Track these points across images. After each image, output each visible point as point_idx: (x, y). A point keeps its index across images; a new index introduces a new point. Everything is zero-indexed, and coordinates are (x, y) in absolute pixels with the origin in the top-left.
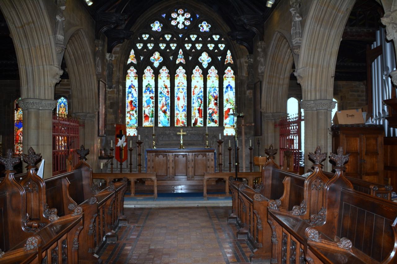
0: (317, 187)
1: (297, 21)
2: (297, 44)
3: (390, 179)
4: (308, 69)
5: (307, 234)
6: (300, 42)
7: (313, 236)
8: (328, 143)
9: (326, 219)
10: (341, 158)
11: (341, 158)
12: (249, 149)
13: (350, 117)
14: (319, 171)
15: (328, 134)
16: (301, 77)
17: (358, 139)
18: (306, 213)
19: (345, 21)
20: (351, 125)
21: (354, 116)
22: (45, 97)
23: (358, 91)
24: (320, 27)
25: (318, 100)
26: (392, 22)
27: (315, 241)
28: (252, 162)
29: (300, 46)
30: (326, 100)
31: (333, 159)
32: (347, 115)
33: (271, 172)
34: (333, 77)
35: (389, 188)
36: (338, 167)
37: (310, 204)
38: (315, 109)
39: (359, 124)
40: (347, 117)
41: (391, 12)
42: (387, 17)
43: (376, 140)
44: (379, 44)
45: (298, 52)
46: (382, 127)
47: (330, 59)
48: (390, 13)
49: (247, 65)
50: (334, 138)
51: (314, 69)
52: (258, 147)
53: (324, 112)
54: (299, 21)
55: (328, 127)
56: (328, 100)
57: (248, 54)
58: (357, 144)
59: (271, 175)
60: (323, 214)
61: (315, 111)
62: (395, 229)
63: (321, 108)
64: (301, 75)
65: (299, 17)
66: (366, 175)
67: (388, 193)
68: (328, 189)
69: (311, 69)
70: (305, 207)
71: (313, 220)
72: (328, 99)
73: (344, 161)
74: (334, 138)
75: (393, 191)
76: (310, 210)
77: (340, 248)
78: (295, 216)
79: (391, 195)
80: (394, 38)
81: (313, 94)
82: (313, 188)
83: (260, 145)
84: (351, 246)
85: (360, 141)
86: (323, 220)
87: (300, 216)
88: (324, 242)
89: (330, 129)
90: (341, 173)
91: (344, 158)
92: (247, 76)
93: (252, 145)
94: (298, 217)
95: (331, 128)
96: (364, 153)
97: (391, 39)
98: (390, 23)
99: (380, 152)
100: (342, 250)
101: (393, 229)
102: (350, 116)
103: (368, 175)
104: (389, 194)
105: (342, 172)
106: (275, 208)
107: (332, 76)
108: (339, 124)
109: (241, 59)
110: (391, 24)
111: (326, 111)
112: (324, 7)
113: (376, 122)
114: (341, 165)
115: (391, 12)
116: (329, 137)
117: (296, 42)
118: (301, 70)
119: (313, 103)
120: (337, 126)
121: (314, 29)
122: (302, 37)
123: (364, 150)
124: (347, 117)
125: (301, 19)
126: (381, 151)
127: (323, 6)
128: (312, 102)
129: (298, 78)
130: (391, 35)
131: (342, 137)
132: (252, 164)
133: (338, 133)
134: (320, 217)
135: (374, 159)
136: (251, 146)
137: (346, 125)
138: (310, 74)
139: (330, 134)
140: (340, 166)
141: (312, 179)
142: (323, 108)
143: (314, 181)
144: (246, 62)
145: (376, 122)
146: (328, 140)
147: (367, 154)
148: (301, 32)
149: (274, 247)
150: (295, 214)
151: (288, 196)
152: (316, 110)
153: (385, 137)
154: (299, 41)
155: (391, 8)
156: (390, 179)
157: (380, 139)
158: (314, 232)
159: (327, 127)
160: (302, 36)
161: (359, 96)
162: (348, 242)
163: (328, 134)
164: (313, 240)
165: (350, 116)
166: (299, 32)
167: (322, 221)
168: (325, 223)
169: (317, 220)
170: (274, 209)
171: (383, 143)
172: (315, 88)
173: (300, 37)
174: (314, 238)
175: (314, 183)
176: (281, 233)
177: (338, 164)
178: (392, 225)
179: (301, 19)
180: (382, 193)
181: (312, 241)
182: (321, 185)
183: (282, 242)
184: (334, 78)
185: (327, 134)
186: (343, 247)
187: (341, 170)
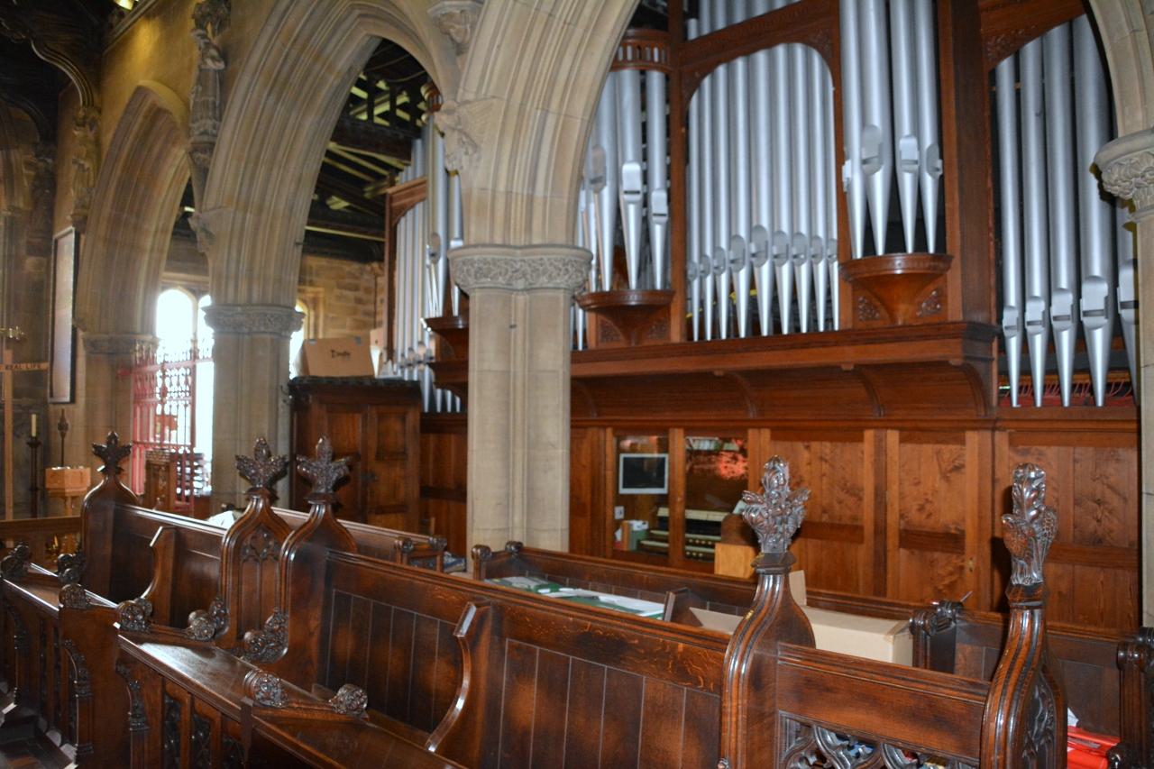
0: (258, 555)
1: (209, 70)
2: (205, 138)
3: (433, 520)
4: (232, 215)
5: (250, 688)
6: (214, 132)
7: (267, 693)
8: (280, 427)
9: (287, 641)
10: (327, 469)
11: (327, 469)
12: (28, 443)
13: (340, 358)
14: (262, 509)
15: (281, 403)
16: (209, 235)
17: (359, 418)
18: (227, 630)
19: (343, 97)
20: (342, 378)
21: (348, 354)
22: (492, 237)
23: (356, 289)
24: (276, 103)
25: (257, 305)
26: (459, 127)
27: (271, 706)
28: (38, 486)
29: (212, 145)
30: (279, 306)
31: (305, 473)
32: (333, 351)
33: (111, 514)
34: (297, 244)
35: (439, 544)
36: (319, 494)
37: (239, 603)
38: (246, 330)
39: (361, 378)
40: (333, 356)
41: (458, 103)
42: (450, 112)
43: (404, 420)
44: (419, 174)
45: (204, 160)
46: (415, 387)
47: (295, 195)
48: (456, 105)
49: (33, 173)
50: (295, 414)
51: (248, 216)
52: (60, 438)
53: (272, 340)
54: (215, 71)
55: (281, 384)
56: (285, 307)
57: (38, 139)
58: (355, 429)
59: (110, 525)
60: (280, 628)
61: (247, 337)
62: (464, 644)
63: (262, 329)
64: (211, 230)
65: (219, 61)
66: (377, 513)
67: (436, 556)
68: (293, 556)
69: (239, 215)
70: (226, 614)
71: (252, 648)
72: (282, 303)
73: (334, 478)
74: (295, 414)
75: (446, 549)
76: (239, 620)
77: (339, 713)
78: (198, 643)
79: (442, 560)
80: (462, 167)
81: (243, 287)
82: (245, 557)
83: (68, 433)
84: (365, 705)
85: (365, 425)
86: (280, 645)
87: (950, 620)
88: (296, 706)
89: (285, 388)
90: (326, 511)
91: (335, 469)
92: (30, 209)
93: (38, 433)
94: (207, 643)
95: (289, 385)
96: (372, 455)
97: (455, 168)
98: (454, 130)
99: (411, 452)
100: (343, 718)
101: (461, 643)
102: (339, 354)
103: (383, 513)
104: (438, 558)
105: (329, 507)
106: (140, 624)
107: (298, 241)
108: (310, 377)
109: (12, 152)
110: (456, 132)
111: (275, 337)
112: (290, 50)
113: (403, 372)
114: (327, 490)
115: (458, 103)
116: (281, 410)
117: (202, 130)
118: (212, 213)
119: (242, 314)
120: (305, 382)
121: (258, 102)
122: (221, 120)
123: (373, 444)
124: (333, 356)
125: (221, 65)
126: (413, 451)
127: (289, 44)
128: (239, 309)
129: (200, 236)
130: (455, 159)
131: (317, 411)
132: (39, 493)
133: (307, 399)
134: (270, 636)
135: (398, 469)
136: (34, 434)
137: (330, 380)
138: (237, 227)
139: (285, 401)
140: (323, 491)
141: (243, 533)
142: (270, 330)
143: (250, 536)
144: (29, 165)
145: (403, 372)
146: (280, 420)
147: (378, 458)
148: (220, 104)
149: (724, 719)
150: (200, 636)
151: (168, 587)
152: (249, 334)
153: (423, 414)
154: (210, 130)
155: (456, 92)
156: (433, 520)
157: (413, 418)
158: (269, 681)
159: (278, 382)
160: (221, 115)
161: (359, 301)
162: (357, 696)
163: (281, 403)
164: (268, 703)
165: (339, 354)
166: (214, 103)
167: (277, 646)
168: (285, 651)
169: (263, 647)
170: (136, 628)
171: (418, 430)
172: (251, 270)
173: (215, 118)
174: (269, 699)
175: (248, 541)
176: (159, 699)
177: (319, 485)
178: (459, 636)
179: (221, 65)
180: (422, 557)
181: (265, 707)
182: (268, 547)
183: (163, 725)
184: (301, 247)
185: (277, 402)
186: (347, 709)
187: (326, 504)
